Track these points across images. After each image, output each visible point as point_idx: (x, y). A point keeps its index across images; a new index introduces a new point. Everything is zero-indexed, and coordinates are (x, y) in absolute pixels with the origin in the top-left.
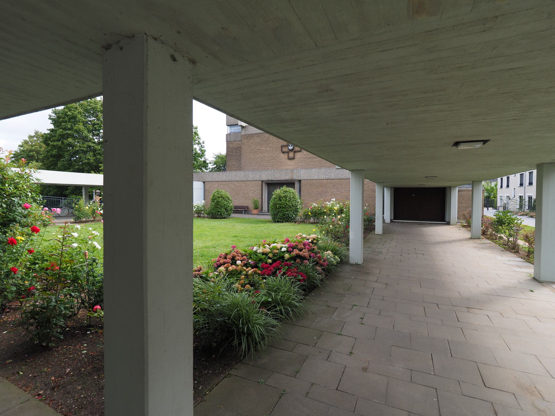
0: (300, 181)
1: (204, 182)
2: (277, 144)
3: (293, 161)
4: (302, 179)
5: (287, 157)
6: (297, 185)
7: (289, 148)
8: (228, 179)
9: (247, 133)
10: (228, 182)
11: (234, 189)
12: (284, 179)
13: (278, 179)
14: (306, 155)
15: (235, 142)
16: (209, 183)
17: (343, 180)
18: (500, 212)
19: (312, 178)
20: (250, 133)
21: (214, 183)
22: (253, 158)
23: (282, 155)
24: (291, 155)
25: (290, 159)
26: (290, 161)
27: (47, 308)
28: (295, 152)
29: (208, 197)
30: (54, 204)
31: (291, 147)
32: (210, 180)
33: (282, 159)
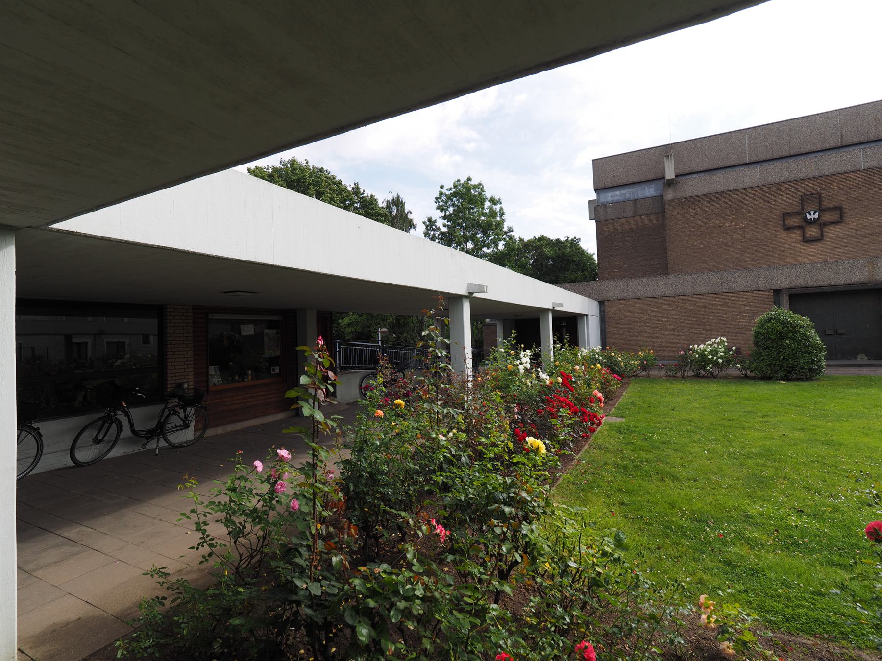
1: (601, 303)
2: (769, 211)
3: (819, 245)
7: (808, 217)
8: (671, 292)
9: (680, 194)
11: (691, 311)
12: (847, 281)
13: (826, 283)
14: (856, 230)
15: (619, 221)
16: (616, 302)
18: (364, 390)
20: (689, 194)
21: (631, 302)
23: (785, 234)
24: (812, 232)
25: (806, 241)
26: (808, 245)
28: (826, 224)
29: (616, 332)
31: (814, 214)
32: (619, 295)
33: (785, 243)
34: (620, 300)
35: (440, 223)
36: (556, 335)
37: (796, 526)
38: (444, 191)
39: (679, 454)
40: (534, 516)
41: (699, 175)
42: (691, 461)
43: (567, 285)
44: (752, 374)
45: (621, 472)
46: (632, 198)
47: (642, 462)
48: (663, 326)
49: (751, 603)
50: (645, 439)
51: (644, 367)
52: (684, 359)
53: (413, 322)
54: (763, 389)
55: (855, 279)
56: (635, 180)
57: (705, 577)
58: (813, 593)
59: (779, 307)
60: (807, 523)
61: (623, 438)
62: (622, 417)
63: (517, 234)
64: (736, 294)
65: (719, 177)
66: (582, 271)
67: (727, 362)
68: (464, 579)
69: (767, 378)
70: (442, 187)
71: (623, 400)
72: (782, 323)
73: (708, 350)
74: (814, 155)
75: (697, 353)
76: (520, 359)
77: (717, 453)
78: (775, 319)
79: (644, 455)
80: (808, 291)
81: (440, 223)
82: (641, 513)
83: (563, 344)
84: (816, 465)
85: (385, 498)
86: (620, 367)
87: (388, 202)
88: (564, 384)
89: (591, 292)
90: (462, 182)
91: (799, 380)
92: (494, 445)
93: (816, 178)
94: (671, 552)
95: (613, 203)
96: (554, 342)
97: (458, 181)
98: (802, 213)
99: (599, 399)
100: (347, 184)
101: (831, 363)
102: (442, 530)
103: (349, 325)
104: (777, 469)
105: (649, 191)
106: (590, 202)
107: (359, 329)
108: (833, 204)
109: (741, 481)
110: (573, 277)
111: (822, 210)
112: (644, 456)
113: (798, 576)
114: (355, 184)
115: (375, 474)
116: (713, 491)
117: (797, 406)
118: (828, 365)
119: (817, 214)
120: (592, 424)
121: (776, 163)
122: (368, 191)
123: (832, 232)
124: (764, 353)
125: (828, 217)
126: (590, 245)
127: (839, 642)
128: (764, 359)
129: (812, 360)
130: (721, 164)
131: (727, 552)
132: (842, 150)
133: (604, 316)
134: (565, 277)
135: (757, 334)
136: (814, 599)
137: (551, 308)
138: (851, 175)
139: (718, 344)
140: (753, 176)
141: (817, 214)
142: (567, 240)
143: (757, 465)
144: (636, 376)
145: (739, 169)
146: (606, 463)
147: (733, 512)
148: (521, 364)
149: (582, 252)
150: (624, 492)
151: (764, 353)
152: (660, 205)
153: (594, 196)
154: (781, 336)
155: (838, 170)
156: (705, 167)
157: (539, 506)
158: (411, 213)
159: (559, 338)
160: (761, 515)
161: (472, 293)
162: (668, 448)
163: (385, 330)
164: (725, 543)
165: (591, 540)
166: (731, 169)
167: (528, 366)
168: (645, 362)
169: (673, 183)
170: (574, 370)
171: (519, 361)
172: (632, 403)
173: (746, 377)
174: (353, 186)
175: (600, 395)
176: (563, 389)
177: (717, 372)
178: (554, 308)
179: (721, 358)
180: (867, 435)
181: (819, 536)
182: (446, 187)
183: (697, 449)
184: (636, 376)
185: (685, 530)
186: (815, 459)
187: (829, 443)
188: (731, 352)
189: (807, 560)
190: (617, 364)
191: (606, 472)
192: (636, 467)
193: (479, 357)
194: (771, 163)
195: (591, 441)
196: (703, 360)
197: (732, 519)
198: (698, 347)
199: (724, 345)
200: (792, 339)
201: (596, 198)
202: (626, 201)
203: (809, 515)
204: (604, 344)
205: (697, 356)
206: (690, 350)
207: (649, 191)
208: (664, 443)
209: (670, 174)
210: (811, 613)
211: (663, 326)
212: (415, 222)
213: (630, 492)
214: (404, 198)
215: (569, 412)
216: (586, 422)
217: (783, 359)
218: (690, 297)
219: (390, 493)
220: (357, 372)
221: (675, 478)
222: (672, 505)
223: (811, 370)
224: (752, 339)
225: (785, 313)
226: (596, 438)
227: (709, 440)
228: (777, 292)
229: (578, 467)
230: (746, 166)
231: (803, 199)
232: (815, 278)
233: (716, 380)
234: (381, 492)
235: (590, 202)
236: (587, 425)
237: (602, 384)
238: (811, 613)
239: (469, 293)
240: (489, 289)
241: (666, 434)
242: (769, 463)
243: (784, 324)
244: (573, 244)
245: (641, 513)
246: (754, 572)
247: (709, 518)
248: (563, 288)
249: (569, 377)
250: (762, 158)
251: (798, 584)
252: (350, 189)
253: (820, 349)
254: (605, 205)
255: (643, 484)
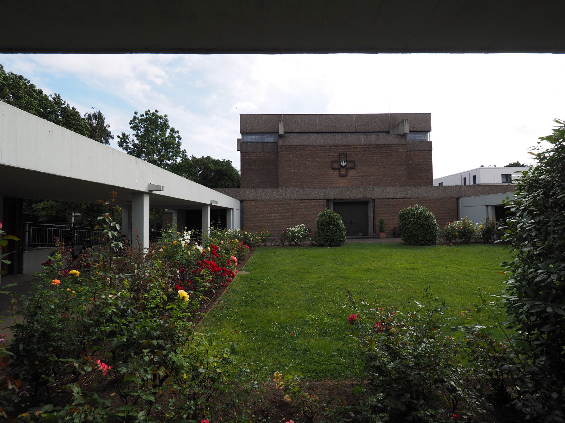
0: (373, 200)
1: (242, 202)
4: (376, 197)
5: (338, 174)
6: (371, 205)
7: (342, 164)
10: (279, 201)
15: (254, 153)
17: (420, 199)
19: (387, 197)
20: (290, 144)
21: (258, 202)
22: (295, 173)
23: (332, 171)
24: (343, 171)
25: (341, 176)
27: (518, 288)
29: (249, 220)
30: (51, 231)
34: (252, 200)
35: (132, 138)
36: (212, 221)
37: (327, 323)
38: (138, 116)
39: (277, 290)
40: (179, 344)
41: (296, 134)
42: (282, 294)
43: (221, 189)
44: (316, 244)
45: (245, 305)
46: (261, 141)
47: (256, 297)
48: (275, 217)
49: (302, 369)
50: (260, 283)
51: (264, 241)
52: (284, 235)
53: (105, 209)
54: (320, 251)
55: (359, 196)
56: (263, 131)
57: (282, 360)
58: (329, 356)
59: (328, 209)
60: (331, 320)
61: (248, 284)
62: (249, 271)
63: (189, 155)
64: (310, 201)
65: (305, 137)
66: (232, 181)
67: (304, 237)
68: (124, 399)
69: (322, 245)
70: (136, 113)
71: (250, 261)
72: (329, 217)
73: (296, 230)
74: (345, 134)
75: (291, 232)
76: (183, 237)
77: (295, 288)
78: (326, 214)
79: (258, 293)
80: (341, 201)
81: (132, 138)
82: (252, 328)
83: (216, 228)
84: (338, 289)
85: (59, 352)
86: (250, 240)
87: (89, 115)
88: (212, 252)
89: (236, 195)
90: (151, 112)
91: (336, 246)
92: (154, 298)
93: (345, 145)
94: (267, 349)
95: (251, 142)
96: (211, 226)
97: (149, 111)
98: (339, 162)
99: (234, 261)
100: (48, 95)
101: (349, 237)
102: (104, 367)
103: (43, 209)
104: (321, 293)
105: (271, 139)
106: (238, 139)
107: (54, 214)
108: (351, 159)
109: (305, 302)
110: (226, 185)
111: (347, 161)
112: (258, 293)
113: (325, 349)
114: (56, 94)
115: (49, 332)
116: (291, 309)
117: (333, 259)
118: (347, 238)
119: (345, 163)
120: (229, 277)
121: (330, 135)
122: (70, 102)
123: (351, 173)
124: (321, 232)
125: (350, 165)
126: (237, 165)
127: (337, 379)
128: (321, 235)
129: (341, 236)
130: (306, 130)
131: (294, 343)
132: (356, 134)
133: (243, 209)
134: (222, 184)
135: (318, 222)
136: (330, 359)
137: (209, 203)
138: (359, 146)
139: (301, 227)
140: (320, 140)
141: (345, 163)
142: (224, 161)
143: (313, 292)
144: (259, 246)
145: (314, 135)
146: (236, 301)
147: (299, 320)
148: (184, 240)
149: (233, 170)
150: (244, 317)
151: (321, 232)
152: (275, 148)
153: (240, 137)
154: (328, 224)
155: (354, 143)
156: (298, 131)
157: (183, 336)
158: (109, 126)
159: (214, 223)
160: (312, 319)
161: (152, 191)
162: (272, 287)
163: (79, 214)
164: (294, 338)
165: (216, 352)
166: (310, 134)
167: (188, 241)
168: (264, 238)
169: (283, 136)
170: (220, 244)
171: (182, 238)
172: (255, 262)
173: (313, 245)
174: (54, 96)
175: (235, 258)
176: (212, 256)
177: (300, 242)
178: (211, 203)
179: (301, 234)
180: (359, 272)
181: (335, 326)
182: (139, 114)
183: (286, 287)
184: (259, 246)
185: (274, 335)
186: (338, 286)
187: (344, 278)
188: (306, 231)
189: (329, 340)
190: (248, 239)
191: (235, 306)
192: (253, 301)
193: (154, 237)
194: (328, 134)
195: (228, 287)
196: (293, 236)
197: (298, 324)
198: (291, 228)
199: (303, 228)
200: (333, 225)
201: (241, 138)
202: (258, 143)
203: (332, 316)
204: (242, 226)
205: (290, 234)
206: (287, 230)
207: (271, 139)
208: (270, 285)
209: (281, 131)
210: (328, 367)
211: (275, 217)
212: (112, 134)
213: (247, 317)
214: (105, 115)
215: (207, 271)
216: (225, 276)
217: (329, 235)
218: (289, 201)
219: (63, 345)
220: (48, 248)
221: (273, 305)
222: (270, 321)
223: (340, 241)
224: (316, 224)
225: (330, 211)
226: (232, 285)
227: (292, 281)
228: (328, 201)
229: (219, 305)
230: (317, 134)
231: (341, 155)
232: (344, 194)
233: (299, 247)
234: (53, 346)
235: (238, 139)
236: (226, 277)
237: (238, 251)
238: (328, 367)
239: (149, 190)
240: (164, 189)
241: (271, 279)
242: (318, 291)
243: (330, 217)
244: (228, 163)
245: (252, 328)
246: (306, 351)
247: (287, 325)
248: (219, 191)
249: (217, 248)
250: (324, 131)
251: (324, 353)
252: (51, 99)
253: (344, 230)
254: (246, 143)
255: (256, 310)
